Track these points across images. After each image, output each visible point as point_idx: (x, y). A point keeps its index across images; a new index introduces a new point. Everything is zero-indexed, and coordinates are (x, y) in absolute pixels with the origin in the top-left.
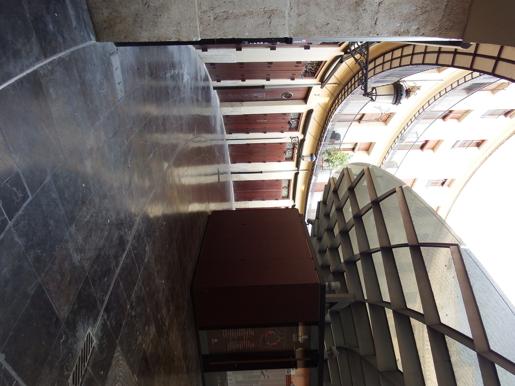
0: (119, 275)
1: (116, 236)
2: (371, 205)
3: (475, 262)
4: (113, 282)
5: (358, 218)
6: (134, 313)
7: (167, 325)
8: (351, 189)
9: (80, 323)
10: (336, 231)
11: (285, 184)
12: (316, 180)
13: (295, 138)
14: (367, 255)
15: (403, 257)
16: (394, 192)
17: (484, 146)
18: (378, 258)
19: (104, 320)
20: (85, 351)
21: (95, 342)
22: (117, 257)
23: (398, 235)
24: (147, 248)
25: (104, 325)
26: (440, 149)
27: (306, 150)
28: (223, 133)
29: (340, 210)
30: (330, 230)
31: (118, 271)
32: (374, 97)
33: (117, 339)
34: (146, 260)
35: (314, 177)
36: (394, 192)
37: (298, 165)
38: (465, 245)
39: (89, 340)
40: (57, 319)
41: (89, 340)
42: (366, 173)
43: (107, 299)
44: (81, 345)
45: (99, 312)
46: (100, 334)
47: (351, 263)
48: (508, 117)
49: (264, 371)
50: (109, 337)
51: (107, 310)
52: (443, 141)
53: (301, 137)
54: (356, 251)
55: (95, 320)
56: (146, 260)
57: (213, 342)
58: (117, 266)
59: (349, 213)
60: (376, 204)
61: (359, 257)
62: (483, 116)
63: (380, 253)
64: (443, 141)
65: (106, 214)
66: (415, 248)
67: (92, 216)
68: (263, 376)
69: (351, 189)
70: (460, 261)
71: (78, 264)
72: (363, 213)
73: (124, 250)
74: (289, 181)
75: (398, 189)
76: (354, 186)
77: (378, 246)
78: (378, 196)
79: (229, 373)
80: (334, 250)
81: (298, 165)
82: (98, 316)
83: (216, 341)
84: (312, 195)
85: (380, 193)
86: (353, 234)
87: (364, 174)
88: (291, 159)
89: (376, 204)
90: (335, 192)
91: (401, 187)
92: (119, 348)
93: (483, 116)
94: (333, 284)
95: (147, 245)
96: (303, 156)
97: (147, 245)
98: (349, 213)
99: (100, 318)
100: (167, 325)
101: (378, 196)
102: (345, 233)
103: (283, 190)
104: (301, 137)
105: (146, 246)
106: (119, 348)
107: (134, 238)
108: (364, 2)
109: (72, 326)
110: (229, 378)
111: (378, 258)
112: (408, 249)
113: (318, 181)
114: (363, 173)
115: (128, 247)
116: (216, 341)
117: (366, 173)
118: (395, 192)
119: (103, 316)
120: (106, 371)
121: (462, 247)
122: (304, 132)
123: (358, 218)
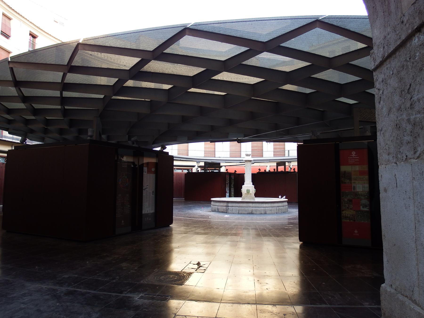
0: (95, 290)
1: (67, 297)
3: (95, 39)
4: (101, 293)
5: (25, 99)
6: (118, 277)
7: (118, 256)
9: (134, 304)
14: (63, 100)
15: (73, 78)
16: (12, 69)
18: (66, 94)
19: (128, 293)
20: (148, 299)
21: (141, 295)
22: (82, 294)
24: (66, 276)
25: (131, 292)
30: (27, 122)
31: (93, 292)
33: (136, 284)
34: (76, 276)
36: (12, 69)
38: (80, 40)
39: (142, 297)
40: (135, 315)
41: (142, 297)
43: (114, 294)
44: (146, 301)
45: (124, 296)
46: (136, 293)
47: (65, 113)
49: (144, 188)
50: (137, 288)
51: (121, 292)
55: (129, 297)
56: (76, 276)
58: (89, 293)
60: (17, 84)
65: (53, 306)
66: (72, 68)
67: (60, 314)
68: (147, 189)
71: (99, 314)
72: (21, 94)
73: (75, 291)
75: (11, 65)
78: (11, 79)
79: (143, 213)
80: (48, 122)
82: (126, 297)
83: (123, 222)
89: (17, 84)
91: (9, 62)
92: (142, 282)
94: (90, 133)
95: (63, 277)
97: (63, 277)
99: (127, 295)
100: (118, 256)
101: (11, 79)
102: (36, 112)
105: (64, 278)
106: (142, 282)
107: (62, 286)
109: (137, 308)
110: (146, 212)
111: (66, 94)
115: (70, 289)
119: (126, 294)
120: (156, 286)
121: (81, 42)
123: (25, 99)
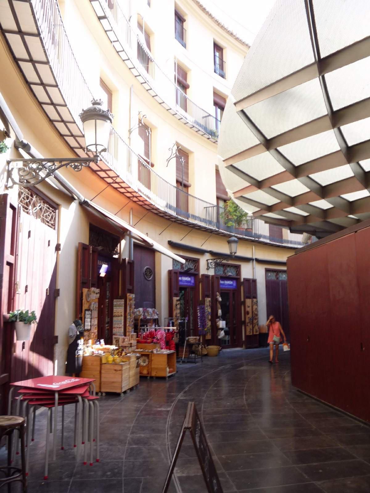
5: (297, 171)
11: (272, 276)
12: (265, 237)
13: (208, 264)
17: (221, 43)
26: (186, 63)
27: (224, 249)
32: (100, 148)
35: (262, 240)
37: (247, 260)
42: (230, 162)
48: (185, 18)
52: (214, 89)
53: (208, 256)
59: (295, 187)
62: (184, 46)
63: (342, 128)
64: (214, 89)
69: (259, 185)
74: (267, 271)
76: (254, 181)
81: (247, 260)
84: (288, 242)
85: (255, 140)
88: (238, 268)
93: (184, 46)
96: (231, 253)
98: (295, 187)
101: (258, 142)
103: (280, 279)
104: (208, 256)
112: (327, 76)
113: (267, 233)
114: (231, 168)
117: (230, 162)
118: (242, 111)
122: (202, 252)
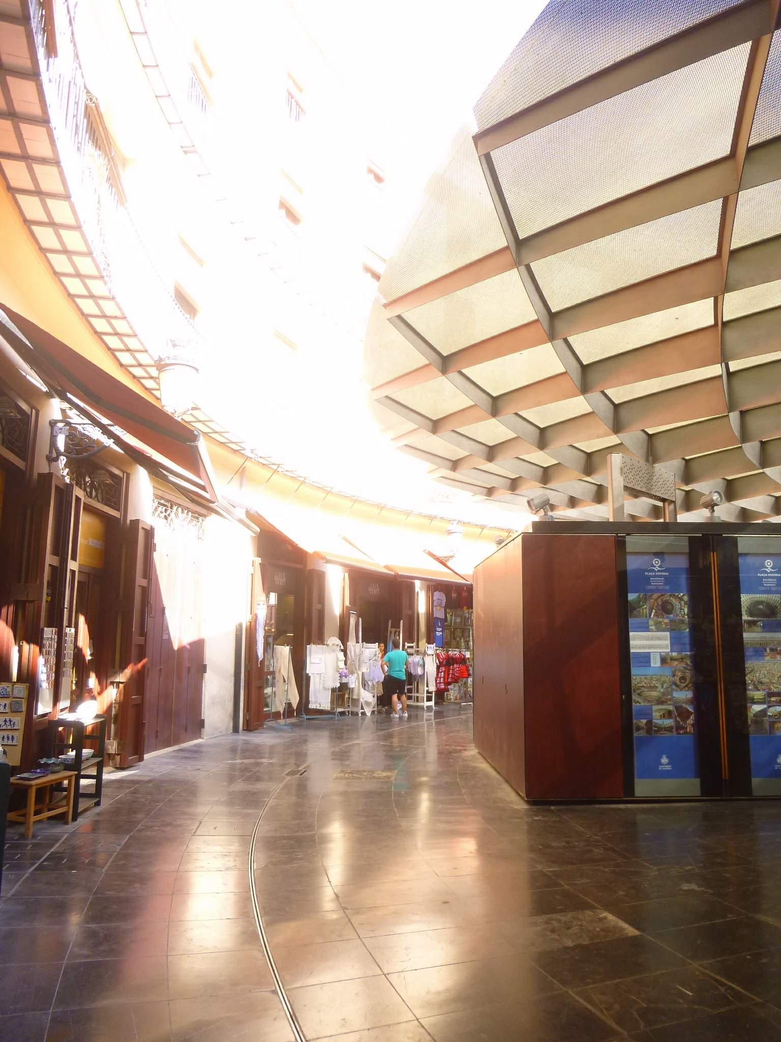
2: (454, 375)
8: (436, 426)
10: (544, 459)
23: (504, 301)
28: (196, 752)
29: (492, 452)
49: (747, 671)
54: (579, 405)
57: (669, 768)
59: (493, 430)
60: (446, 363)
61: (595, 395)
69: (436, 426)
70: (391, 402)
77: (547, 349)
80: (591, 463)
83: (664, 760)
85: (419, 359)
86: (545, 414)
87: (387, 397)
90: (455, 465)
98: (493, 430)
108: (417, 1039)
116: (664, 760)
118: (399, 317)
